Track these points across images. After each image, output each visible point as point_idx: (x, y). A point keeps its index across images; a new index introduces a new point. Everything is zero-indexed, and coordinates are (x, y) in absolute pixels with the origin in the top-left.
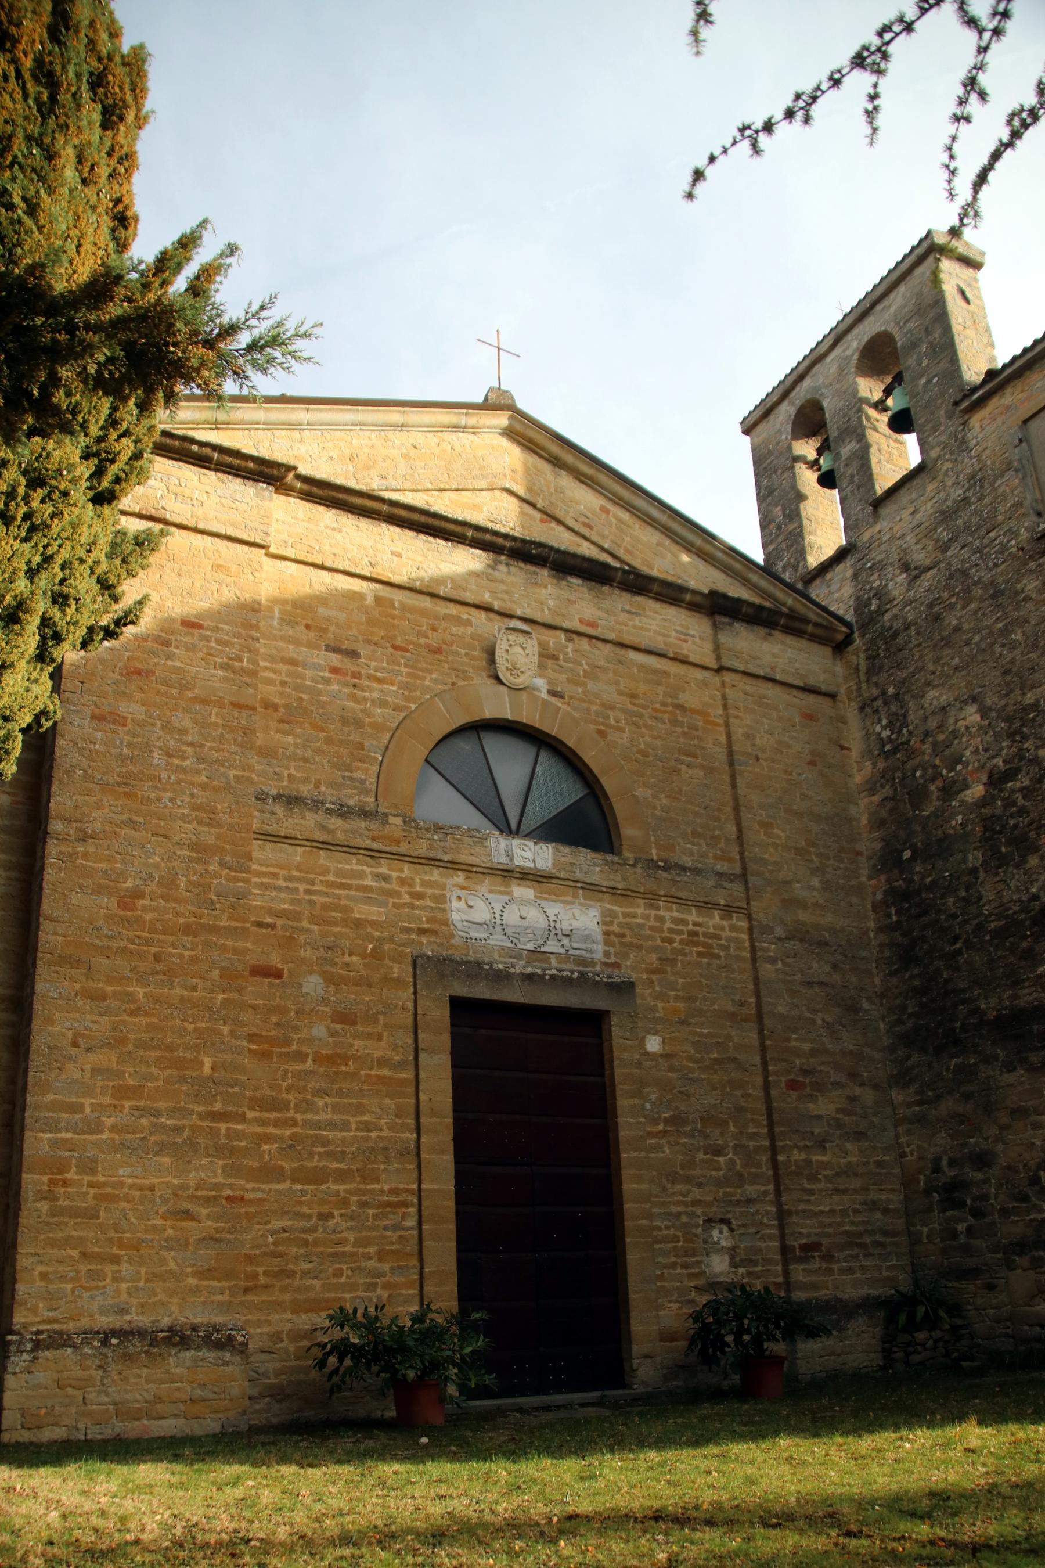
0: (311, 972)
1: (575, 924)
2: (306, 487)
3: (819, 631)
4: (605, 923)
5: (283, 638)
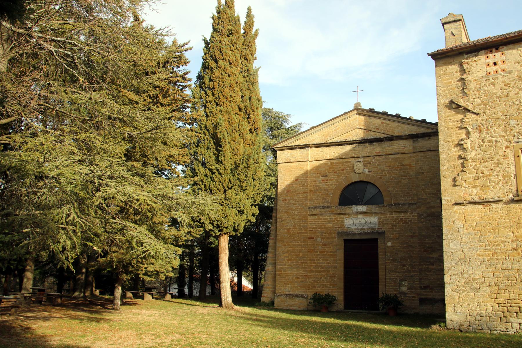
1: (372, 221)
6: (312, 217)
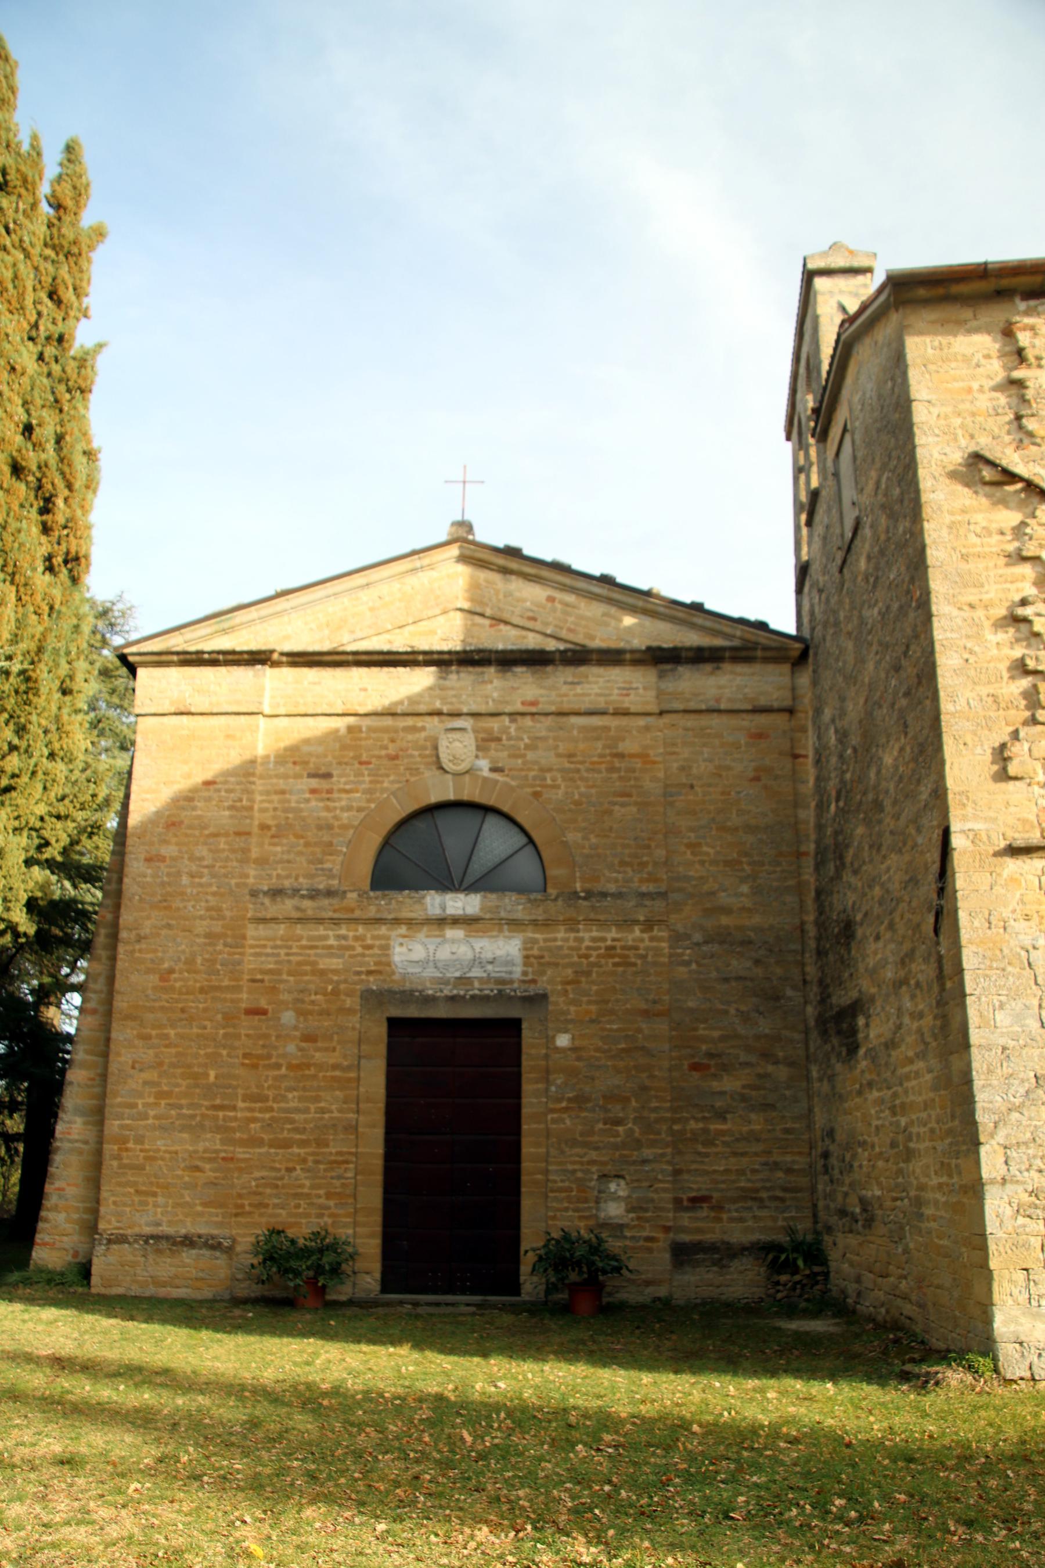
0: (287, 1009)
1: (499, 953)
2: (290, 659)
3: (769, 654)
5: (277, 776)
6: (262, 931)
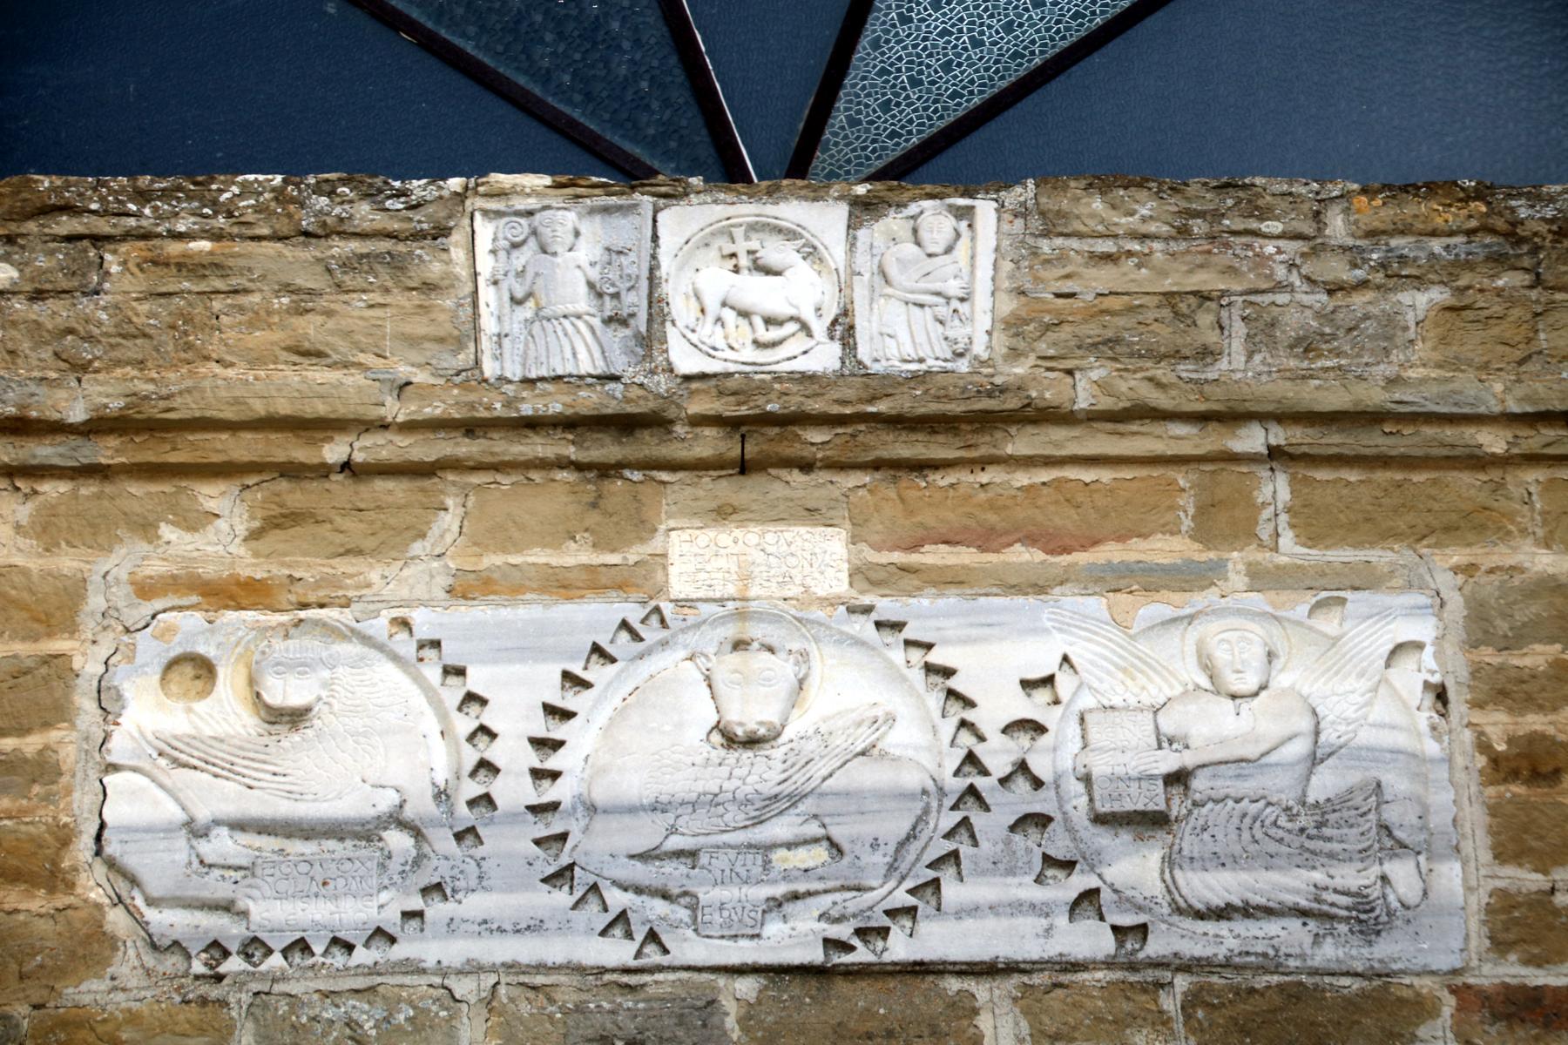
1: (1213, 728)
4: (1502, 690)
